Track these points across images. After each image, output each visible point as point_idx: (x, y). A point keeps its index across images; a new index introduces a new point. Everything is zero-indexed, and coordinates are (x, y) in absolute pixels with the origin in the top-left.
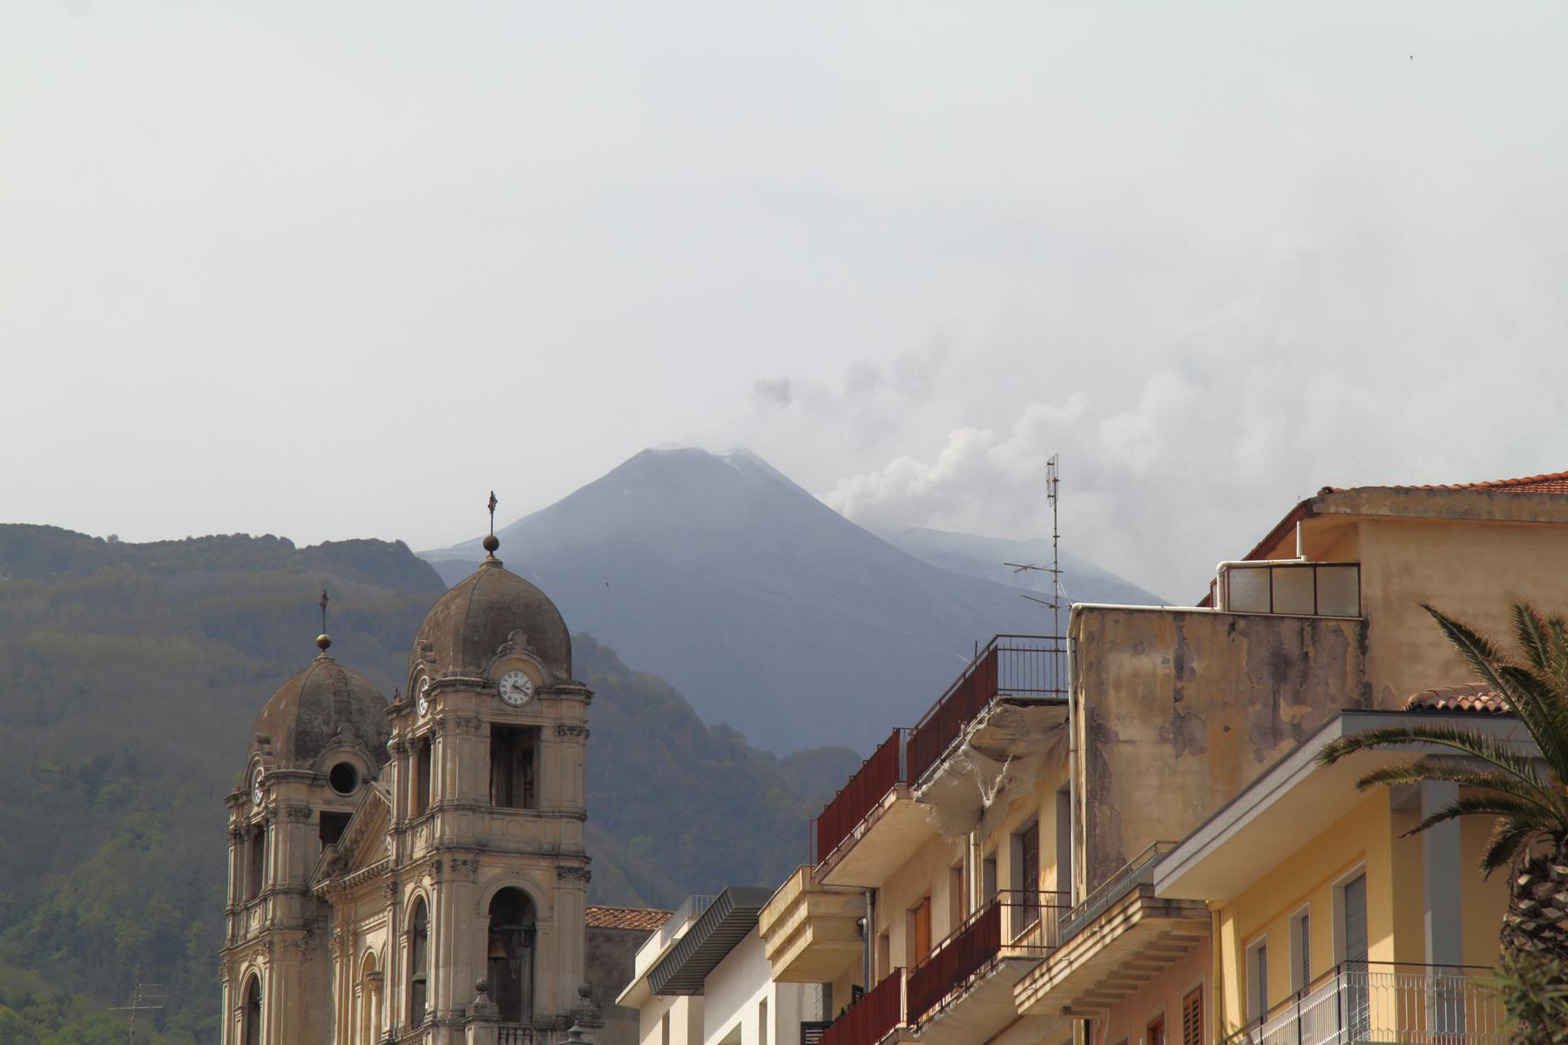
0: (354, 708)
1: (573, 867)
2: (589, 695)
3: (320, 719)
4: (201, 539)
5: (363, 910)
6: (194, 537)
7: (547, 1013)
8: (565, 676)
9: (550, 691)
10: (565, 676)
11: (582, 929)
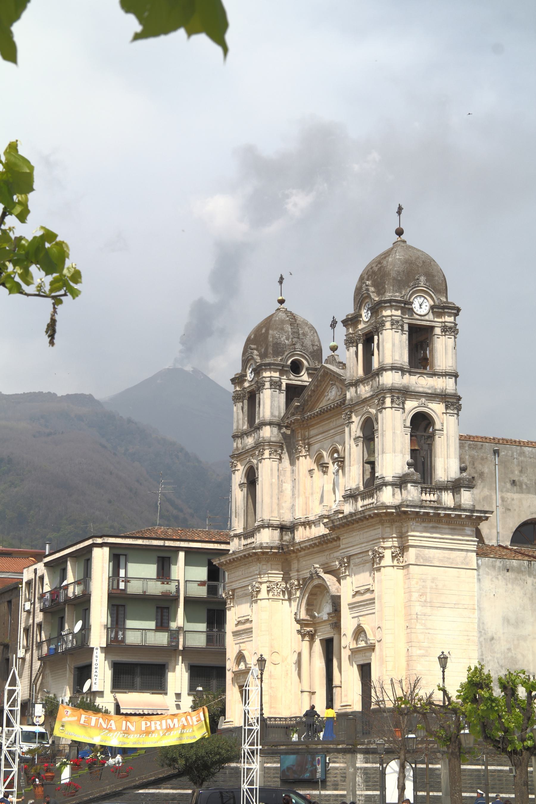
0: (301, 332)
1: (452, 402)
2: (458, 310)
3: (284, 337)
4: (28, 393)
5: (313, 432)
6: (26, 392)
7: (442, 480)
8: (445, 300)
9: (439, 309)
10: (445, 300)
11: (458, 436)
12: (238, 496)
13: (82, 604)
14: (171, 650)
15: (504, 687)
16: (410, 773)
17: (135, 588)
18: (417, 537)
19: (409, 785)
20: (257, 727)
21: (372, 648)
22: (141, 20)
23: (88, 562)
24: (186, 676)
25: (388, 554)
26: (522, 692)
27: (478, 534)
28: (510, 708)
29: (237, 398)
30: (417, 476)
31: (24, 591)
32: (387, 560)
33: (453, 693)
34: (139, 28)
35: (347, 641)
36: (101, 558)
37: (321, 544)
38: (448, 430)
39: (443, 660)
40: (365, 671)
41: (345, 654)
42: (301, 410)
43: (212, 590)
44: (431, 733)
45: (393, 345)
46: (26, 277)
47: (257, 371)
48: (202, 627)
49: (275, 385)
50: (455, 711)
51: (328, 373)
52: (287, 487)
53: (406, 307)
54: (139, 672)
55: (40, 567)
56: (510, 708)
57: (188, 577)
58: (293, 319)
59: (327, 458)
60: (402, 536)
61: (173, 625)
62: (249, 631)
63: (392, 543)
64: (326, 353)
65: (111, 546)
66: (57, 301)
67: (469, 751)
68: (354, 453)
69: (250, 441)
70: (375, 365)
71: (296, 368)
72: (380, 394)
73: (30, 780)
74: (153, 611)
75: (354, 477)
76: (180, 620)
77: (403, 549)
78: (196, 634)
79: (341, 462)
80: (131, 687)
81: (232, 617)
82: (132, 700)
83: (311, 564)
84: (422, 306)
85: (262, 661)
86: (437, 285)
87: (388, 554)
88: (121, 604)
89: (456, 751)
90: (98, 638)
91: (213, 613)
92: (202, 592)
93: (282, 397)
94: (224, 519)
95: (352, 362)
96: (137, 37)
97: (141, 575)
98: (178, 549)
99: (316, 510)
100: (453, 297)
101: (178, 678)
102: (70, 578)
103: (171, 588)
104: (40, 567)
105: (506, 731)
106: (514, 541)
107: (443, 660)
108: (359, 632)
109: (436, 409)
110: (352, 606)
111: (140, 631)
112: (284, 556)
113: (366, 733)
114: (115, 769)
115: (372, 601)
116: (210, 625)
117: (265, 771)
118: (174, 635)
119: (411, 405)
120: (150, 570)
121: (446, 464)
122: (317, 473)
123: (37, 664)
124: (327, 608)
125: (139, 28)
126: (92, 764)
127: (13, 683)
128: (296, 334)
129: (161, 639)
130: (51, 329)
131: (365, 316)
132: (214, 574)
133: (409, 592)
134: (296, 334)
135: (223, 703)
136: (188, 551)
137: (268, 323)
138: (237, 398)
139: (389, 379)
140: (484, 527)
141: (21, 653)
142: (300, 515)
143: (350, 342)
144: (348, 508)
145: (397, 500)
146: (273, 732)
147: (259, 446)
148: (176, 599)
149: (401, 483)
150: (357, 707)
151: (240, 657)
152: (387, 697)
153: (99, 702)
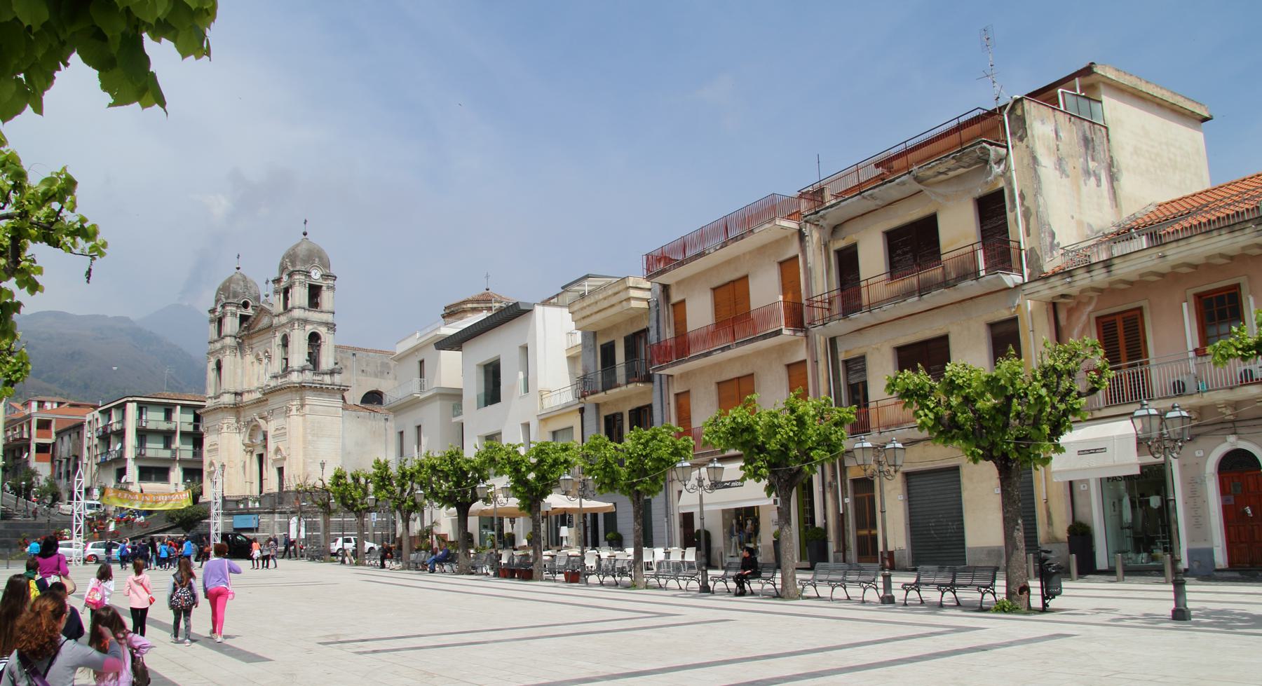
1: (331, 327)
9: (326, 276)
12: (211, 375)
13: (121, 434)
14: (173, 460)
15: (353, 478)
16: (303, 523)
17: (151, 426)
18: (311, 399)
19: (303, 530)
20: (220, 501)
21: (284, 459)
22: (112, 96)
23: (124, 411)
24: (181, 474)
25: (294, 408)
26: (363, 481)
27: (343, 398)
28: (356, 488)
29: (212, 321)
30: (311, 367)
31: (86, 426)
32: (294, 412)
33: (327, 482)
34: (112, 101)
35: (270, 456)
36: (132, 409)
37: (258, 402)
38: (328, 342)
39: (323, 465)
40: (281, 470)
41: (270, 462)
42: (248, 328)
43: (196, 427)
44: (314, 502)
45: (300, 295)
46: (74, 244)
47: (223, 306)
48: (191, 447)
49: (234, 314)
50: (327, 491)
51: (263, 309)
52: (239, 371)
53: (307, 274)
54: (154, 472)
55: (96, 413)
56: (356, 488)
57: (182, 420)
58: (245, 279)
59: (261, 356)
60: (302, 399)
61: (173, 446)
62: (216, 450)
63: (297, 402)
64: (263, 298)
65: (138, 402)
66: (93, 258)
67: (335, 511)
68: (277, 352)
69: (218, 345)
70: (290, 306)
71: (246, 305)
72: (292, 322)
73: (91, 530)
74: (161, 439)
75: (277, 366)
76: (177, 442)
77: (303, 406)
78: (186, 451)
79: (269, 358)
80: (149, 480)
81: (207, 442)
82: (150, 486)
83: (248, 412)
84: (316, 275)
85: (223, 466)
86: (325, 264)
87: (294, 408)
88: (143, 435)
89: (327, 510)
90: (130, 453)
91: (196, 439)
92: (190, 428)
93: (237, 321)
94: (202, 387)
95: (277, 303)
96: (110, 105)
97: (155, 419)
98: (176, 405)
99: (256, 384)
100: (333, 271)
101: (176, 474)
102: (114, 419)
103: (171, 426)
104: (96, 413)
105: (354, 500)
106: (362, 402)
107: (323, 465)
108: (278, 450)
109: (322, 331)
110: (274, 437)
111: (155, 449)
112: (237, 409)
113: (280, 503)
114: (141, 524)
115: (285, 434)
116: (195, 447)
117: (225, 524)
118: (174, 452)
119: (309, 328)
120: (161, 415)
121: (326, 361)
122: (256, 363)
123: (95, 467)
124: (261, 437)
125: (112, 101)
126: (127, 521)
127: (80, 477)
128: (246, 286)
129: (167, 454)
130: (89, 273)
131: (285, 278)
132: (197, 418)
133: (305, 429)
134: (246, 286)
135: (201, 488)
136: (183, 406)
137: (230, 280)
138: (212, 321)
139: (297, 313)
140: (346, 394)
141: (85, 460)
142: (246, 387)
143: (276, 292)
144: (273, 383)
145: (300, 380)
146: (231, 506)
147: (223, 348)
148: (175, 432)
149: (302, 370)
150: (276, 490)
151: (212, 464)
152: (291, 484)
153: (131, 488)
